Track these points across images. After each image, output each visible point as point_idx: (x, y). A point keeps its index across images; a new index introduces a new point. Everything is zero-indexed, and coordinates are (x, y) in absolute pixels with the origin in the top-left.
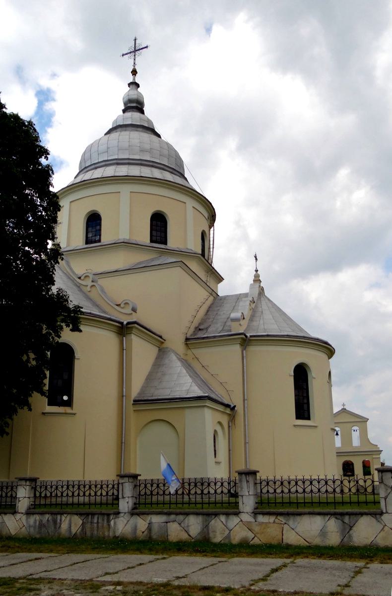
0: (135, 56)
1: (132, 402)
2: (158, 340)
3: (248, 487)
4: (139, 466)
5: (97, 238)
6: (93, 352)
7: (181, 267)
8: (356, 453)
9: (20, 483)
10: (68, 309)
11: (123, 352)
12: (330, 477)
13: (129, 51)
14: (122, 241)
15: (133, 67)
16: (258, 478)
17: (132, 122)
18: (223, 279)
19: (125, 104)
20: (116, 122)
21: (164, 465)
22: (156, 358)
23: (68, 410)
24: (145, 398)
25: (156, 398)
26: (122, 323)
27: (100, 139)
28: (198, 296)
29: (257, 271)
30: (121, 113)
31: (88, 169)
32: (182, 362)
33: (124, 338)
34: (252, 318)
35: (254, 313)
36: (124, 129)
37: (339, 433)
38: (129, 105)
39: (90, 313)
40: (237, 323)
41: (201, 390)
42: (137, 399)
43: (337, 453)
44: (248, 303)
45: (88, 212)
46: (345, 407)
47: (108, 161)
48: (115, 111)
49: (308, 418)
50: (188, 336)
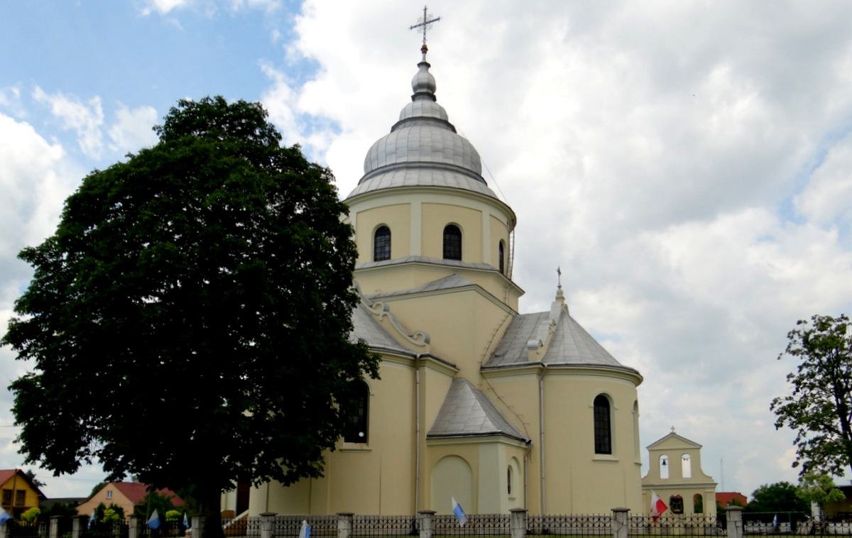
0: (425, 29)
1: (426, 437)
2: (451, 368)
3: (519, 522)
4: (431, 503)
5: (387, 256)
6: (388, 394)
8: (686, 486)
9: (340, 517)
10: (237, 106)
11: (417, 386)
12: (640, 515)
14: (413, 260)
16: (629, 515)
17: (422, 113)
18: (524, 292)
19: (415, 89)
20: (405, 112)
21: (454, 504)
22: (450, 389)
23: (364, 446)
24: (440, 433)
25: (450, 433)
26: (415, 356)
28: (495, 318)
29: (560, 287)
30: (411, 101)
31: (375, 172)
32: (477, 393)
33: (418, 371)
34: (552, 344)
35: (554, 338)
36: (414, 122)
37: (667, 462)
39: (384, 348)
40: (534, 352)
41: (494, 424)
42: (431, 434)
43: (643, 486)
44: (548, 327)
46: (675, 431)
47: (396, 164)
48: (401, 99)
49: (609, 452)
50: (483, 366)
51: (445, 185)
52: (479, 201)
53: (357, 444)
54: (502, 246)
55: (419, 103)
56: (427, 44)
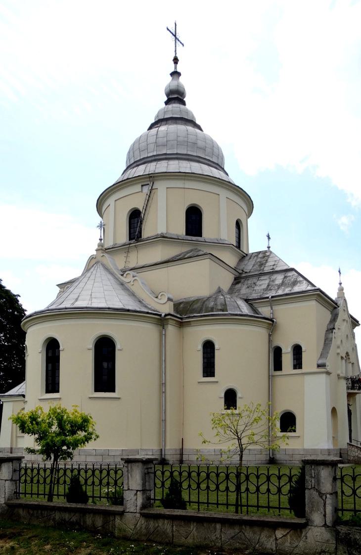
13: (174, 42)
15: (174, 55)
19: (168, 95)
29: (340, 284)
30: (164, 105)
38: (170, 97)
45: (131, 208)
47: (147, 157)
48: (157, 104)
51: (190, 172)
52: (222, 187)
53: (106, 393)
54: (238, 225)
55: (170, 106)
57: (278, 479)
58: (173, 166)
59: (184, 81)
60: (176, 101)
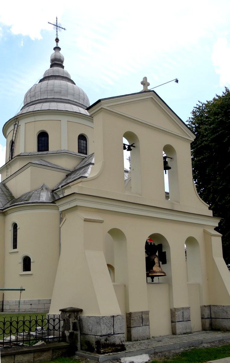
0: (60, 27)
7: (32, 166)
27: (31, 88)
31: (28, 105)
45: (38, 131)
47: (41, 99)
48: (45, 66)
51: (72, 111)
56: (58, 37)
57: (17, 323)
58: (45, 106)
59: (62, 53)
60: (55, 66)
